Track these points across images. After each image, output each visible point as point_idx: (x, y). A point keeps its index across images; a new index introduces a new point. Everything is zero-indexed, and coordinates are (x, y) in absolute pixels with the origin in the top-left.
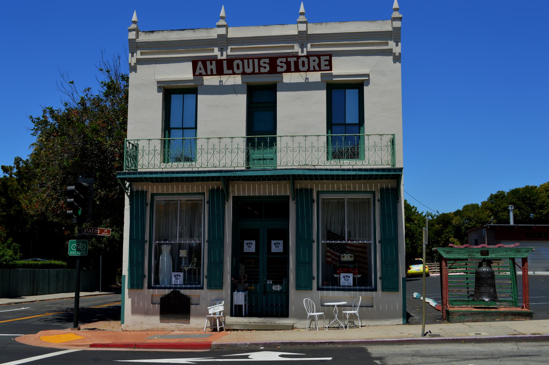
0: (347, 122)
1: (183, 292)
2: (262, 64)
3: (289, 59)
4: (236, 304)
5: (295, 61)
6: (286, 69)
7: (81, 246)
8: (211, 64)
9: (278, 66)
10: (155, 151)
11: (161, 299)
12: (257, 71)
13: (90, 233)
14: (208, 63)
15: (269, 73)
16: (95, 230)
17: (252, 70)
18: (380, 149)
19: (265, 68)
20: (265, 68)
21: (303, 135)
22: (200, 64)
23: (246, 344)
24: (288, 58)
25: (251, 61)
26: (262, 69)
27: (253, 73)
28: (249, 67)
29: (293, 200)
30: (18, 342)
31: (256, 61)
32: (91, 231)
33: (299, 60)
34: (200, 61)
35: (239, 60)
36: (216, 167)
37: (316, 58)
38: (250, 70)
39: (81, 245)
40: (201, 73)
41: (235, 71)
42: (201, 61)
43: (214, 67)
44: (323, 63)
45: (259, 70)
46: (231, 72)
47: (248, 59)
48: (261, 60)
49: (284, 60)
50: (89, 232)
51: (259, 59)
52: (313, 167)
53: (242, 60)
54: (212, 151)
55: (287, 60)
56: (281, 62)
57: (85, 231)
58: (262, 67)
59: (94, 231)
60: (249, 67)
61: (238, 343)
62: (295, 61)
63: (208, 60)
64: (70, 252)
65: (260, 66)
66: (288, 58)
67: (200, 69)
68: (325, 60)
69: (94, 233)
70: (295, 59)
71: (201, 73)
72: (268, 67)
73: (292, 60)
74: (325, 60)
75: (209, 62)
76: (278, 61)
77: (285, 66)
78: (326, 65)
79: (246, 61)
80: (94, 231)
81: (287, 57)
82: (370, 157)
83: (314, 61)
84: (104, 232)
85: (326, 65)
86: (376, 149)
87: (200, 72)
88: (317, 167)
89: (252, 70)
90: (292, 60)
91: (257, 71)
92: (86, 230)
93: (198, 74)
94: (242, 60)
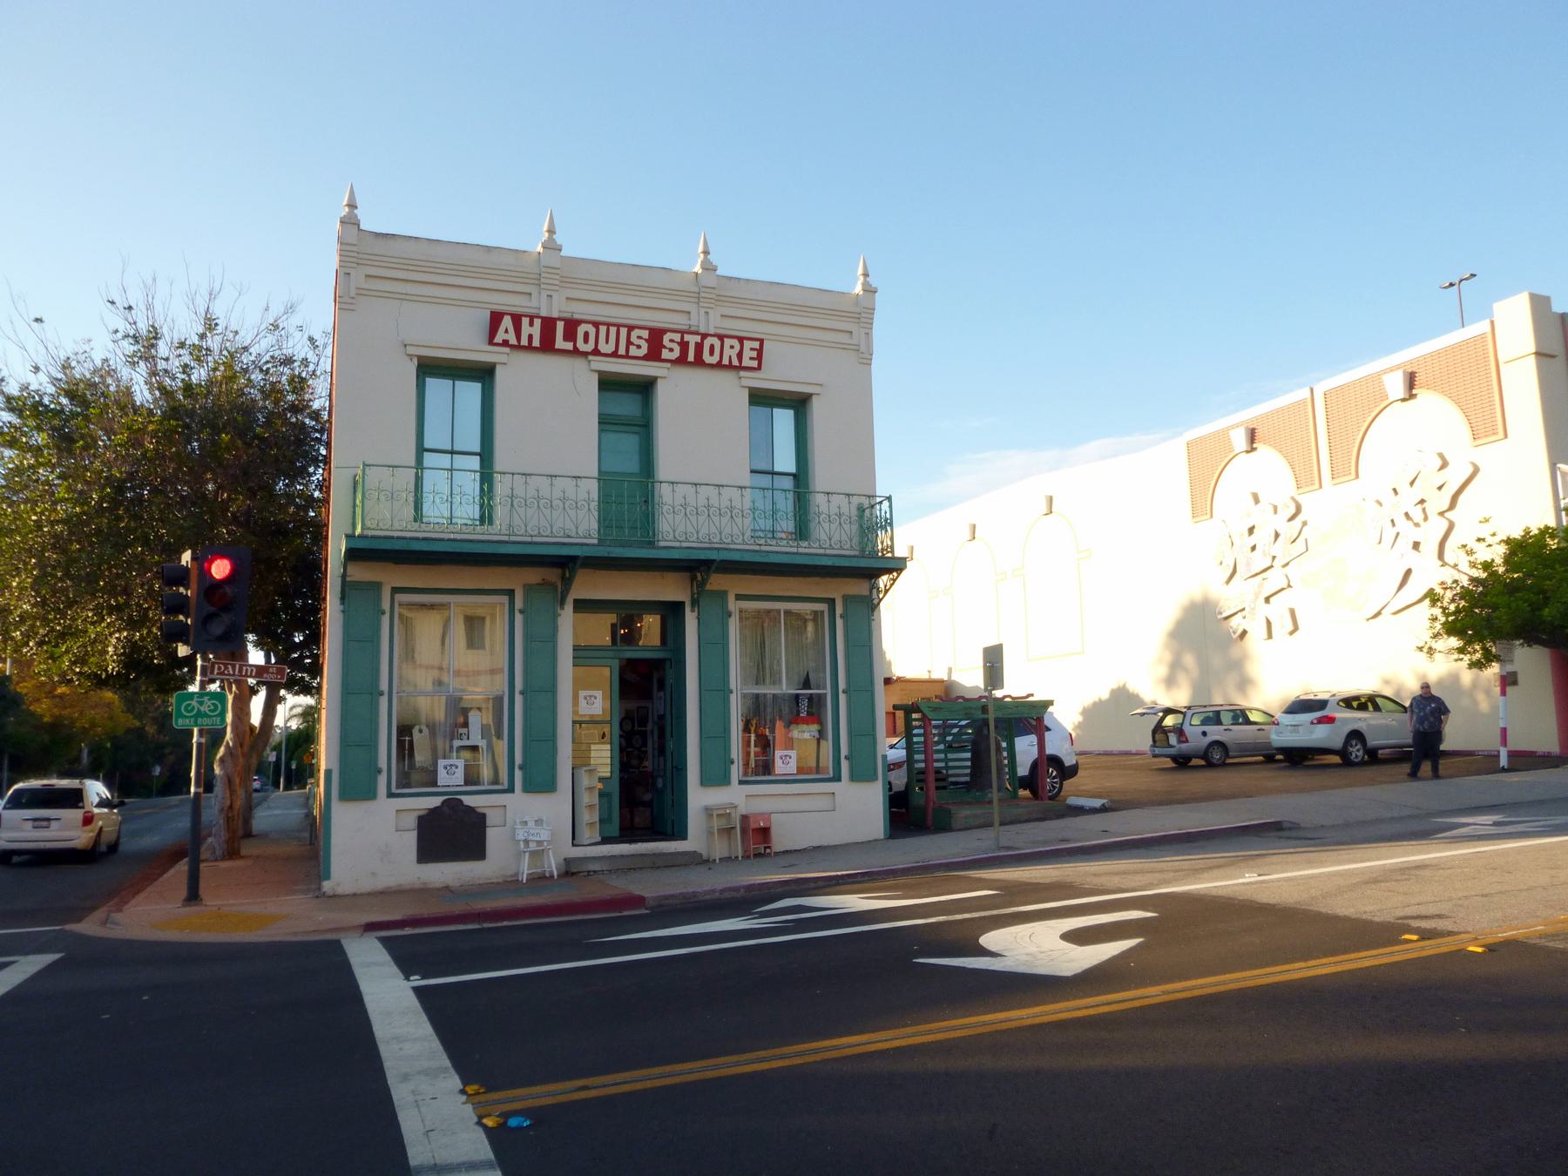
0: (776, 469)
1: (468, 800)
2: (634, 339)
3: (687, 338)
4: (744, 813)
5: (696, 343)
6: (678, 355)
7: (209, 706)
8: (531, 324)
9: (665, 347)
10: (588, 501)
11: (421, 819)
12: (622, 351)
13: (229, 675)
14: (525, 321)
15: (645, 358)
16: (244, 668)
17: (593, 347)
18: (549, 506)
19: (639, 347)
20: (639, 347)
21: (389, 464)
22: (507, 322)
23: (713, 891)
24: (685, 335)
25: (613, 330)
26: (632, 348)
27: (615, 354)
28: (607, 342)
29: (693, 611)
30: (1346, 919)
31: (624, 331)
32: (234, 671)
33: (705, 342)
34: (508, 314)
35: (590, 326)
36: (569, 537)
37: (736, 343)
38: (610, 348)
39: (209, 703)
40: (508, 341)
41: (578, 345)
42: (512, 315)
43: (536, 331)
44: (747, 354)
45: (627, 350)
46: (569, 346)
47: (608, 325)
48: (633, 330)
49: (677, 337)
50: (226, 672)
51: (631, 328)
52: (529, 539)
53: (721, 338)
54: (556, 502)
55: (682, 338)
56: (672, 341)
57: (216, 671)
58: (633, 344)
59: (240, 671)
60: (607, 342)
61: (699, 890)
62: (696, 343)
63: (526, 316)
64: (177, 721)
65: (629, 343)
66: (685, 335)
67: (506, 331)
68: (752, 349)
69: (241, 675)
70: (698, 339)
71: (508, 341)
72: (645, 346)
73: (692, 340)
74: (752, 349)
75: (626, 329)
76: (666, 338)
77: (677, 349)
78: (751, 358)
79: (603, 329)
80: (240, 671)
81: (683, 333)
82: (699, 526)
83: (732, 347)
84: (268, 673)
85: (751, 358)
86: (515, 503)
87: (506, 337)
88: (535, 539)
89: (614, 349)
90: (692, 340)
91: (622, 351)
92: (219, 668)
93: (501, 342)
94: (596, 325)
